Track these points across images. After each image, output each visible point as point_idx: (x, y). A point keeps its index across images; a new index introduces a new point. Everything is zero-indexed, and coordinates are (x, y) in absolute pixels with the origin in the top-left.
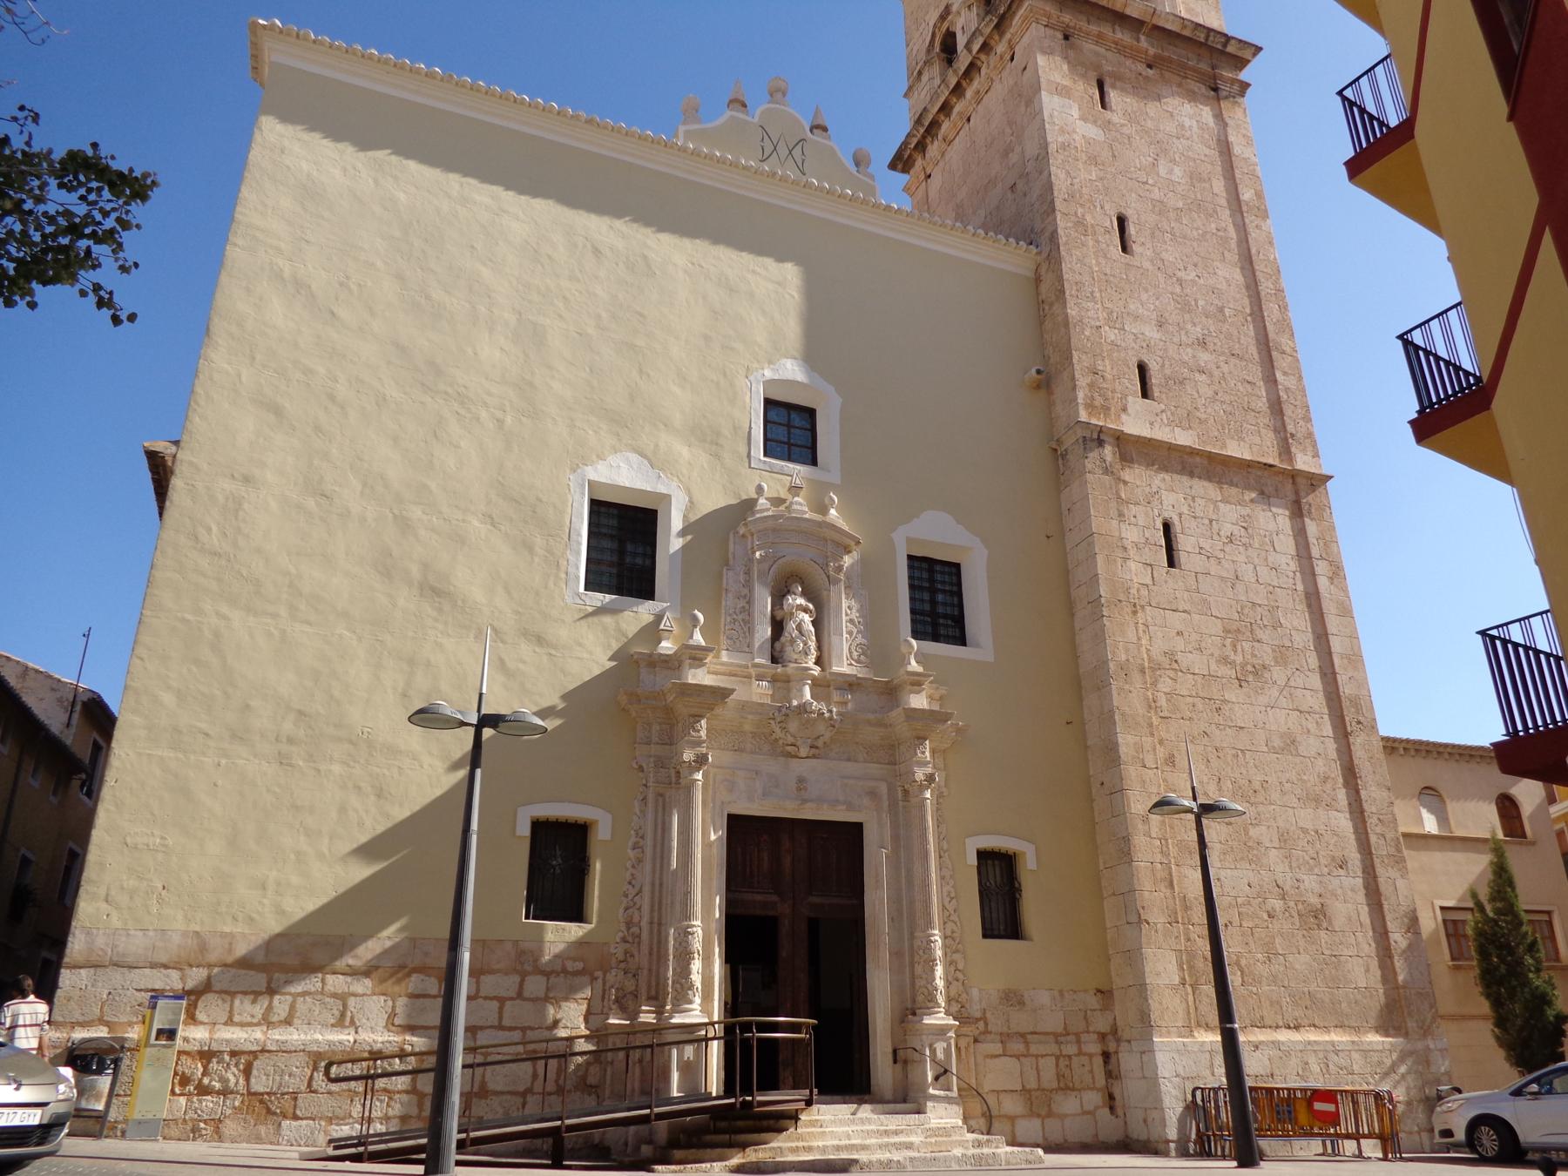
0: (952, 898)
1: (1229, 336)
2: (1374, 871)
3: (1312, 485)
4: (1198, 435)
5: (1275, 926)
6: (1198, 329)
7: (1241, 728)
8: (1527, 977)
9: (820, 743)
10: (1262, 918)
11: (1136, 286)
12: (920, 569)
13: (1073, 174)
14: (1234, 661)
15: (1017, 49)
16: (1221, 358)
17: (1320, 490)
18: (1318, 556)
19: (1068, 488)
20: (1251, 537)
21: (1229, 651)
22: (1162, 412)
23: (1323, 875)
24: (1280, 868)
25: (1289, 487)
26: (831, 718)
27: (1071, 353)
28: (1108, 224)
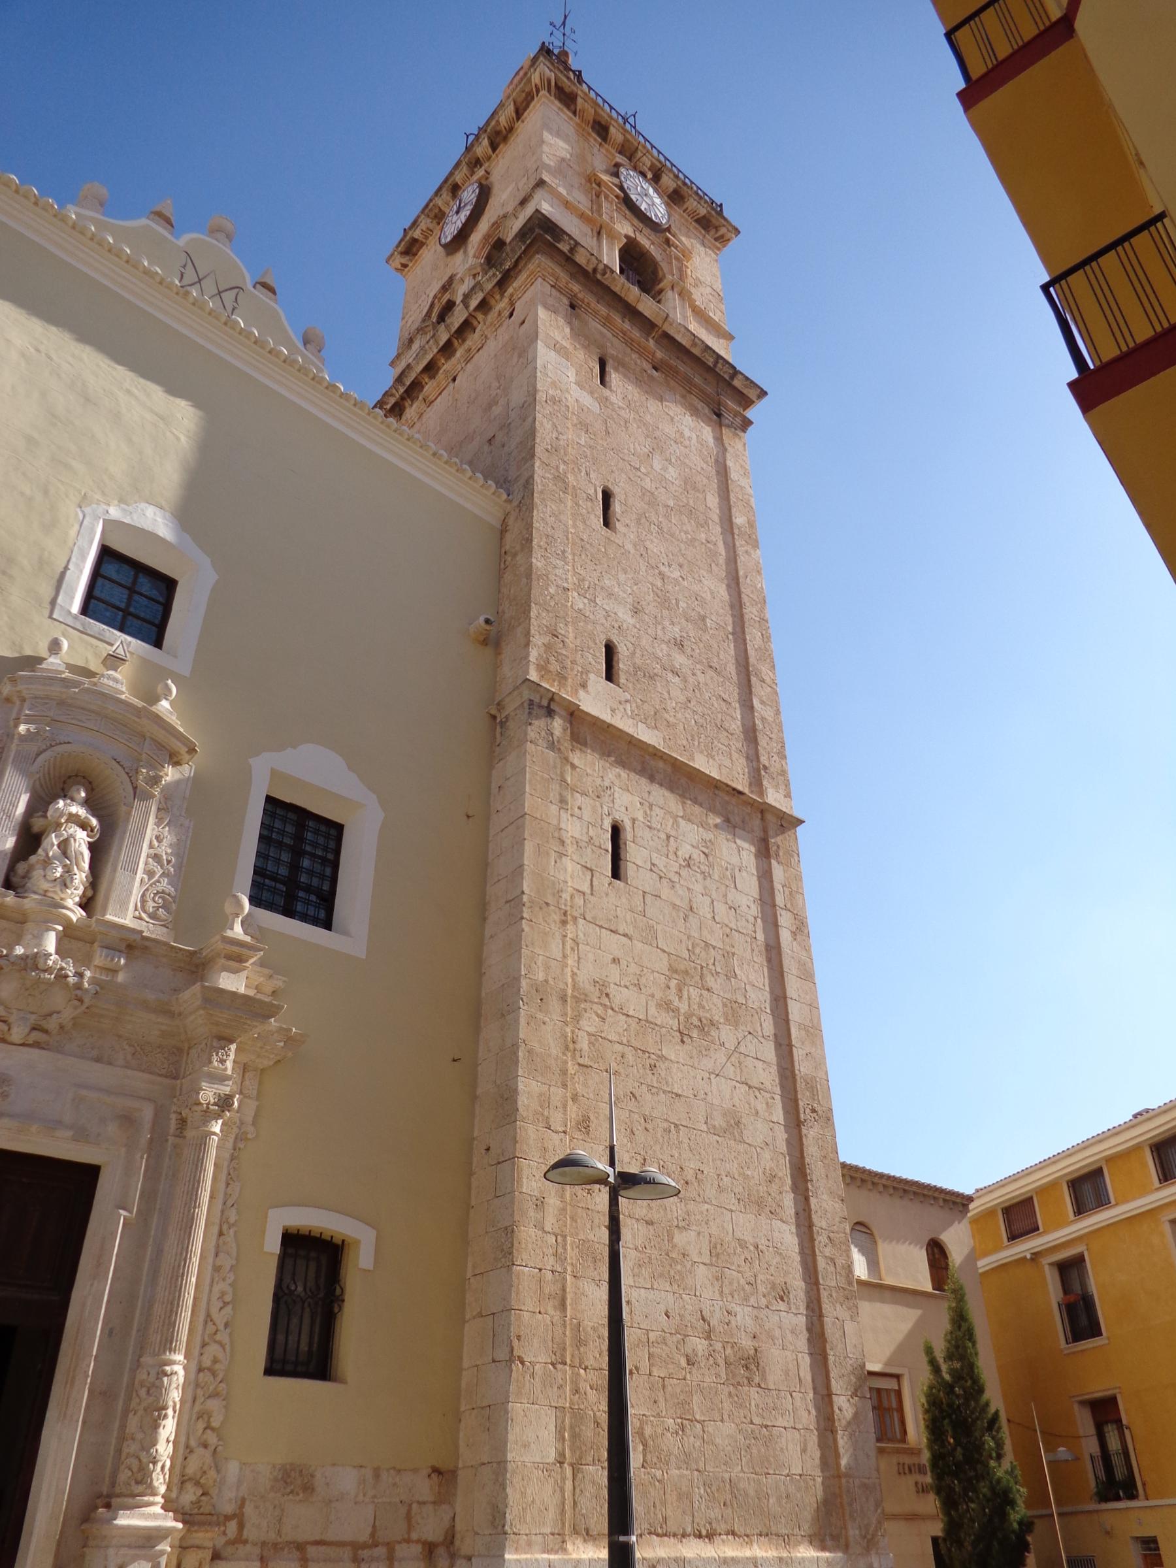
0: (226, 1304)
1: (709, 647)
2: (820, 1308)
3: (782, 825)
4: (664, 739)
5: (694, 1377)
6: (677, 629)
7: (678, 1095)
8: (987, 1466)
9: (52, 1024)
10: (679, 1366)
11: (615, 563)
12: (284, 820)
13: (560, 430)
14: (678, 1009)
15: (518, 306)
16: (698, 666)
17: (789, 833)
18: (782, 906)
19: (501, 763)
20: (711, 866)
21: (672, 995)
22: (627, 701)
23: (759, 1308)
24: (707, 1294)
25: (757, 822)
26: (78, 986)
27: (529, 606)
28: (591, 492)
